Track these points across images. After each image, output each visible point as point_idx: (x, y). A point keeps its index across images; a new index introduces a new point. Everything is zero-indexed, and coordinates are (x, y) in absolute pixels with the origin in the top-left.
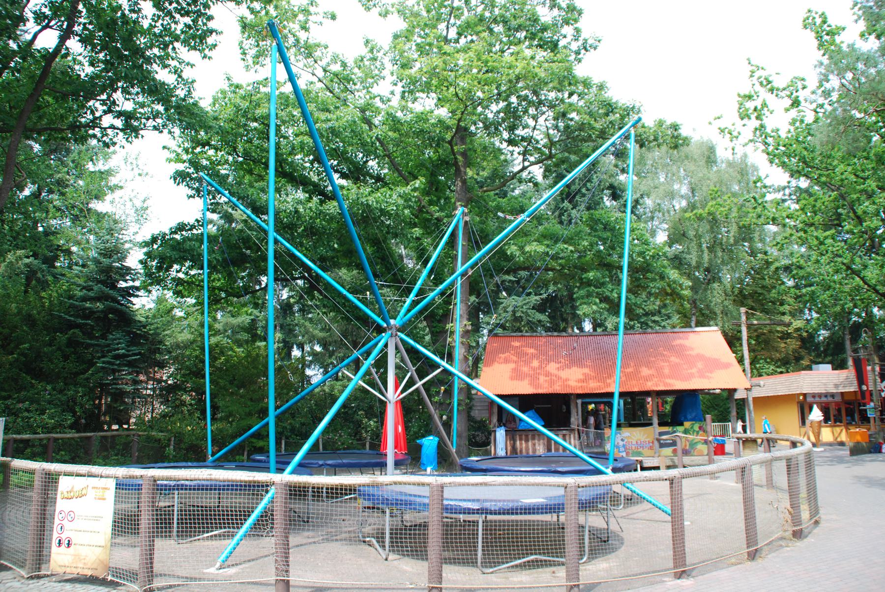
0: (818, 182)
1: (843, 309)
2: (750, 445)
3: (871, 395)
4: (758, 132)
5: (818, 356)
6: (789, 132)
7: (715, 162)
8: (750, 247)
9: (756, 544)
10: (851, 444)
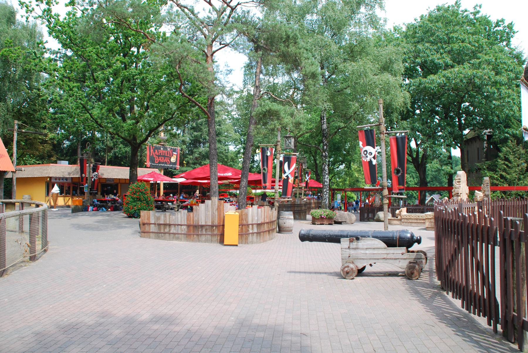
0: (77, 55)
1: (77, 130)
2: (10, 206)
3: (87, 180)
4: (46, 13)
5: (62, 156)
6: (65, 19)
7: (14, 23)
8: (29, 84)
9: (5, 266)
10: (73, 207)
